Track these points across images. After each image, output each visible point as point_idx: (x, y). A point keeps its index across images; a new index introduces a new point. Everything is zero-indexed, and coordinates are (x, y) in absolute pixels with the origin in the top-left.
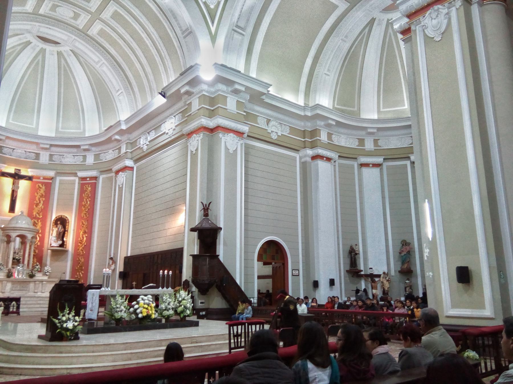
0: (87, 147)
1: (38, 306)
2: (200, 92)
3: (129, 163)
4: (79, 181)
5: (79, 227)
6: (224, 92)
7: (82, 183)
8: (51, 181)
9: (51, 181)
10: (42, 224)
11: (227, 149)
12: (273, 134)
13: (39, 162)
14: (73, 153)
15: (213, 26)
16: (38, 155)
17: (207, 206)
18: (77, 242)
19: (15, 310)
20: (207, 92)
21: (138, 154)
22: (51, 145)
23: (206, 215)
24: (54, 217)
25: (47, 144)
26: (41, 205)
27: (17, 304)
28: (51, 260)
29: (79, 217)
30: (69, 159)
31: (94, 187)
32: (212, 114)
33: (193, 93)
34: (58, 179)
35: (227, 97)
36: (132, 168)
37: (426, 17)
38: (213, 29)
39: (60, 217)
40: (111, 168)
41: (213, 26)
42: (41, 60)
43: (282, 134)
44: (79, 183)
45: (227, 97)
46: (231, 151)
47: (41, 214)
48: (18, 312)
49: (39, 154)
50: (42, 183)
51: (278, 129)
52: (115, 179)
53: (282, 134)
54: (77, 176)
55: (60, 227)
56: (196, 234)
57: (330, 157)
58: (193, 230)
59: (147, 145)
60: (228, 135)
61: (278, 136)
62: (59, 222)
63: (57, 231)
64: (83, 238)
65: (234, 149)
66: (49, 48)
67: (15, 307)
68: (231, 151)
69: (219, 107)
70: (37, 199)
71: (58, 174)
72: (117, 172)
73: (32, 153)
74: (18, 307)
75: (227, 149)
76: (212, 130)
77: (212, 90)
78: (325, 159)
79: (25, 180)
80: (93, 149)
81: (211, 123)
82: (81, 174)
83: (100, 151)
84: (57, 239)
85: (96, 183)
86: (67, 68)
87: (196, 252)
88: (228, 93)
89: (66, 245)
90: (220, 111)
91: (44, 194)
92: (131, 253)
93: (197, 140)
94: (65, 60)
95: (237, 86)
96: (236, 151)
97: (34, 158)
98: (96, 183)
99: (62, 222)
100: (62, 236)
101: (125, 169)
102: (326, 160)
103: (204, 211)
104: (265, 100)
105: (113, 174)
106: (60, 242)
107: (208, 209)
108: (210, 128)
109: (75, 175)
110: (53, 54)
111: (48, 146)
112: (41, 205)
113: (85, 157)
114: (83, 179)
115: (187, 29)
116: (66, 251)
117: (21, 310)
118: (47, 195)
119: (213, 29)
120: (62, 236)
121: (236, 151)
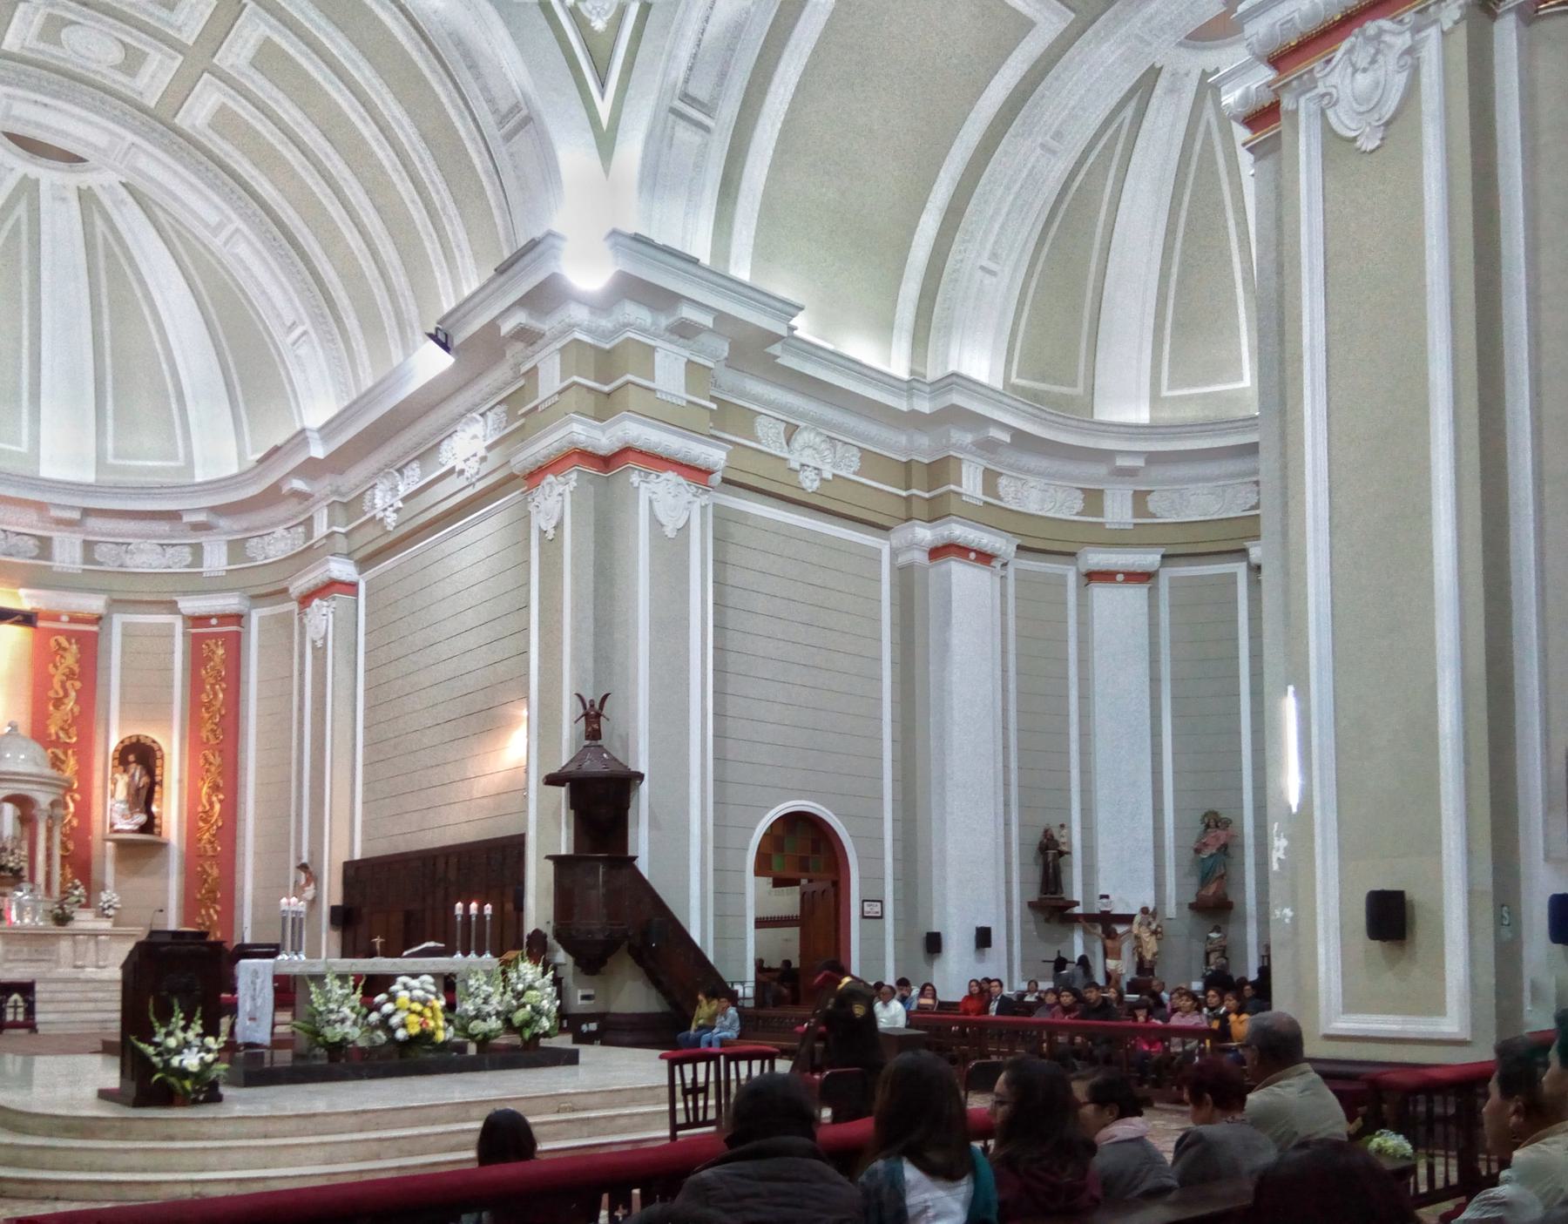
0: (201, 518)
1: (91, 1006)
2: (564, 333)
3: (341, 569)
4: (185, 627)
5: (195, 773)
6: (643, 331)
7: (194, 635)
8: (95, 628)
9: (95, 628)
10: (78, 761)
11: (656, 523)
12: (807, 473)
13: (51, 567)
14: (161, 537)
15: (603, 96)
16: (45, 545)
17: (597, 706)
18: (195, 819)
19: (20, 1018)
20: (589, 331)
21: (369, 540)
22: (87, 512)
23: (594, 734)
24: (114, 742)
25: (72, 508)
26: (70, 704)
27: (25, 1001)
28: (117, 872)
29: (194, 742)
30: (147, 557)
31: (235, 645)
32: (604, 407)
33: (541, 335)
34: (118, 621)
35: (653, 349)
36: (351, 587)
37: (1334, 62)
38: (604, 109)
39: (134, 740)
40: (285, 584)
41: (603, 96)
42: (24, 219)
43: (834, 475)
44: (184, 634)
45: (653, 349)
46: (670, 531)
47: (73, 730)
48: (30, 1025)
49: (50, 539)
50: (69, 635)
51: (823, 459)
52: (301, 620)
53: (834, 475)
54: (177, 612)
55: (137, 771)
56: (563, 792)
57: (988, 550)
58: (552, 780)
59: (397, 511)
60: (658, 477)
61: (823, 480)
62: (131, 758)
63: (129, 785)
64: (211, 804)
65: (681, 524)
66: (48, 175)
67: (21, 1010)
68: (670, 531)
69: (628, 383)
70: (57, 685)
71: (117, 604)
72: (306, 600)
73: (26, 538)
74: (30, 1010)
75: (656, 523)
76: (606, 462)
77: (606, 323)
78: (972, 555)
79: (13, 623)
80: (224, 523)
81: (604, 439)
82: (192, 605)
83: (247, 530)
84: (130, 809)
85: (238, 634)
86: (117, 249)
87: (565, 847)
88: (657, 336)
89: (160, 826)
90: (633, 397)
91: (76, 669)
92: (364, 850)
93: (560, 495)
94: (108, 220)
95: (687, 313)
96: (685, 529)
97: (34, 554)
98: (238, 634)
99: (141, 755)
100: (144, 797)
101: (330, 587)
102: (976, 560)
103: (588, 723)
104: (778, 361)
105: (293, 606)
106: (142, 818)
107: (598, 715)
108: (602, 453)
109: (172, 607)
110: (64, 199)
111: (76, 515)
112: (70, 704)
113: (197, 550)
114: (199, 620)
115: (515, 108)
116: (162, 846)
117: (39, 1018)
118: (88, 671)
119: (604, 109)
120: (144, 797)
121: (685, 529)
